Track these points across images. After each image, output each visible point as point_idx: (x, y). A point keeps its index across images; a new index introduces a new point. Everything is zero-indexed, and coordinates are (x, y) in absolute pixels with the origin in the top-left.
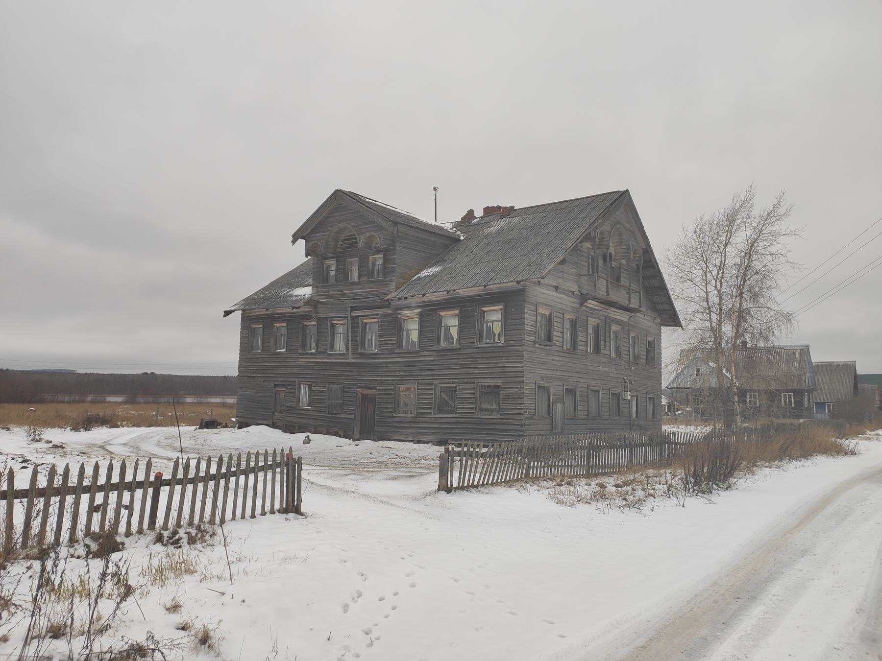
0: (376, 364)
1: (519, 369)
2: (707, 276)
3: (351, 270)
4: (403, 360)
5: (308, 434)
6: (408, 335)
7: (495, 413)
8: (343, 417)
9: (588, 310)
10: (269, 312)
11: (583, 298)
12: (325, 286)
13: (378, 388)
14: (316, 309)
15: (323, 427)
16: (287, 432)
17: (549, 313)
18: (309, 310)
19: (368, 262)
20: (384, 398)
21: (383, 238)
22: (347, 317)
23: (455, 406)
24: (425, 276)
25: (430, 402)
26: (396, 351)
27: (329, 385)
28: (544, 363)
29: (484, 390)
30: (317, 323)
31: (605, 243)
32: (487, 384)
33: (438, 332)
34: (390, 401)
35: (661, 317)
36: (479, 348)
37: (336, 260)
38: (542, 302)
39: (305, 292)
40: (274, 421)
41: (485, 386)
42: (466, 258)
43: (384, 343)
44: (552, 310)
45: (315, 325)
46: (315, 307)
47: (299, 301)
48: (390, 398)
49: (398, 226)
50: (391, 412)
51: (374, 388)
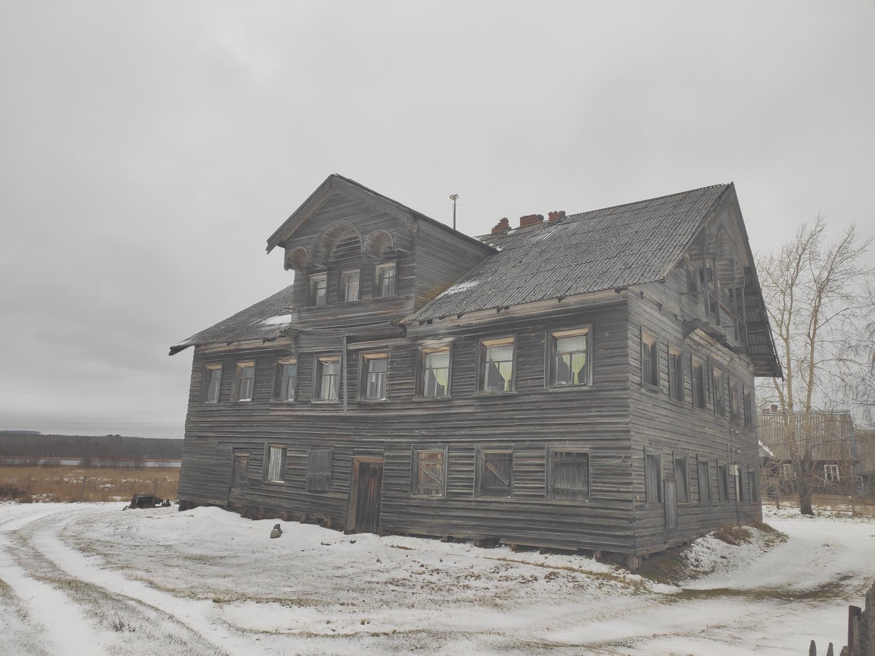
0: (382, 418)
1: (620, 427)
2: (784, 318)
3: (349, 286)
4: (426, 413)
5: (278, 521)
6: (433, 378)
7: (579, 498)
8: (332, 496)
9: (692, 344)
10: (232, 347)
11: (688, 327)
12: (310, 310)
13: (386, 454)
14: (296, 341)
15: (303, 511)
16: (249, 518)
17: (652, 344)
18: (287, 343)
19: (373, 275)
20: (394, 470)
21: (398, 236)
22: (341, 351)
23: (510, 483)
24: (455, 293)
25: (469, 477)
26: (414, 400)
27: (312, 449)
28: (651, 419)
29: (559, 459)
30: (298, 362)
31: (711, 252)
32: (564, 450)
33: (481, 370)
34: (405, 474)
35: (753, 363)
36: (550, 393)
37: (328, 274)
38: (646, 324)
39: (285, 320)
40: (230, 500)
41: (561, 453)
42: (513, 269)
43: (396, 387)
44: (657, 338)
45: (294, 364)
46: (296, 339)
47: (273, 331)
48: (405, 470)
49: (419, 222)
50: (406, 492)
51: (379, 454)
